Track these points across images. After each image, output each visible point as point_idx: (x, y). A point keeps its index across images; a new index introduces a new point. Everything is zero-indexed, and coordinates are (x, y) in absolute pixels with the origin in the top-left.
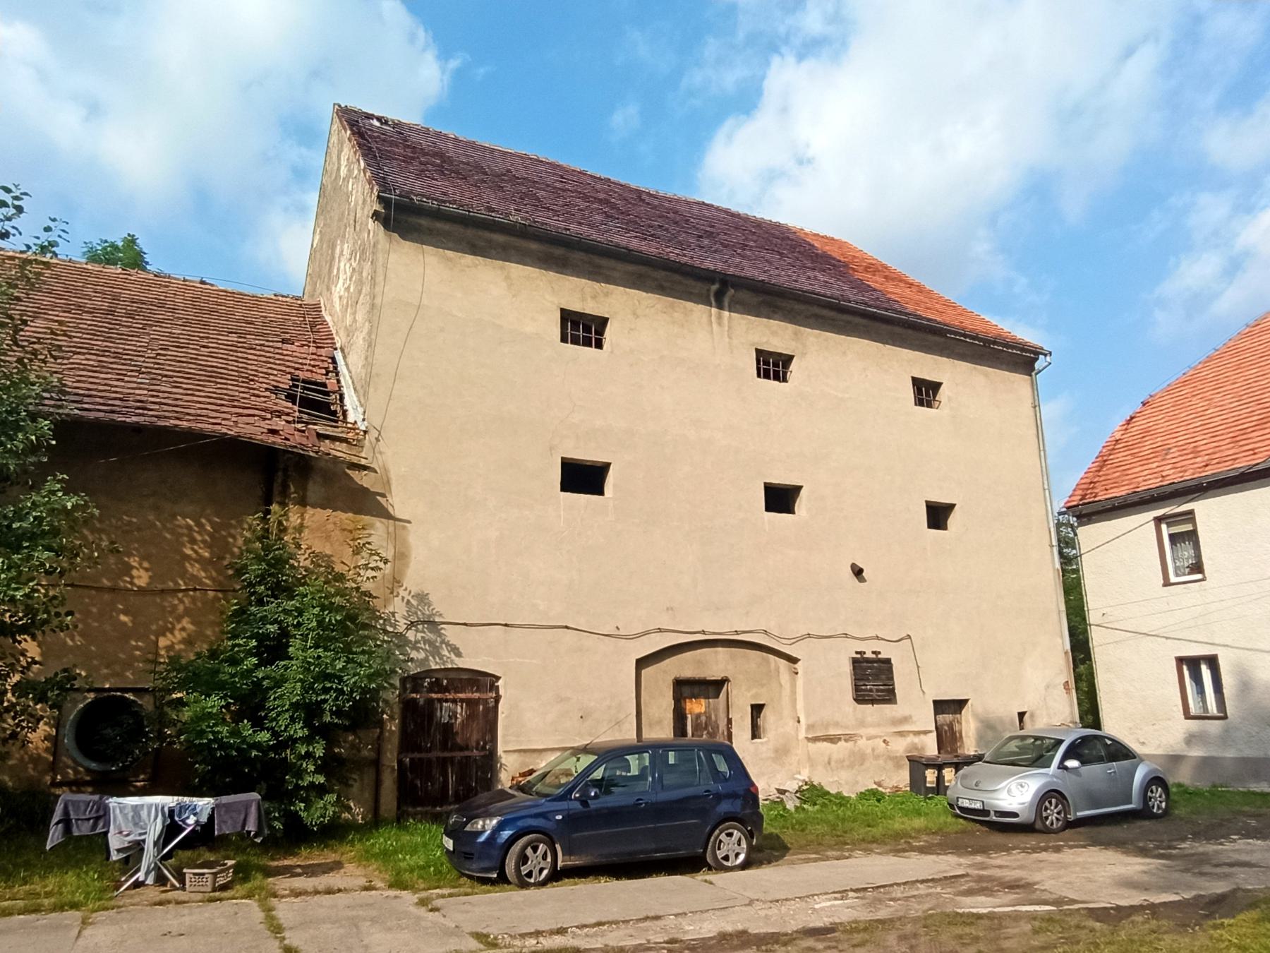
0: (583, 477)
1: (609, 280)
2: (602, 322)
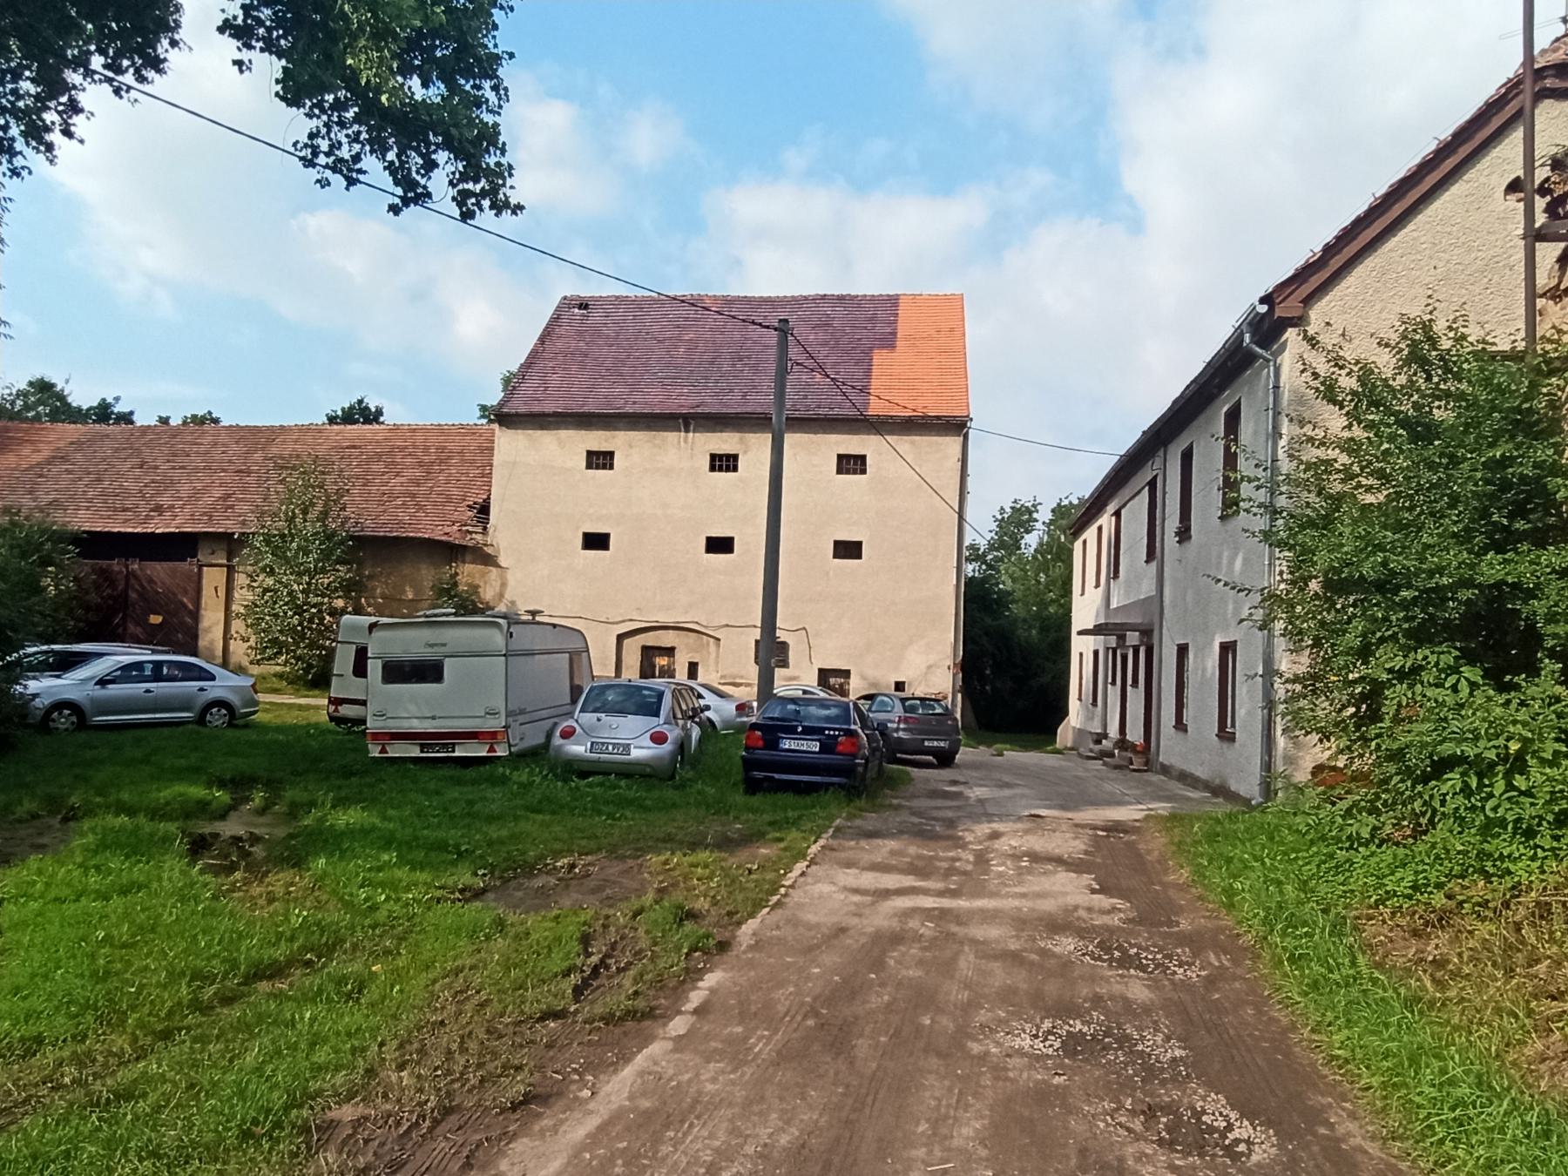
0: (596, 541)
1: (616, 429)
2: (611, 454)
